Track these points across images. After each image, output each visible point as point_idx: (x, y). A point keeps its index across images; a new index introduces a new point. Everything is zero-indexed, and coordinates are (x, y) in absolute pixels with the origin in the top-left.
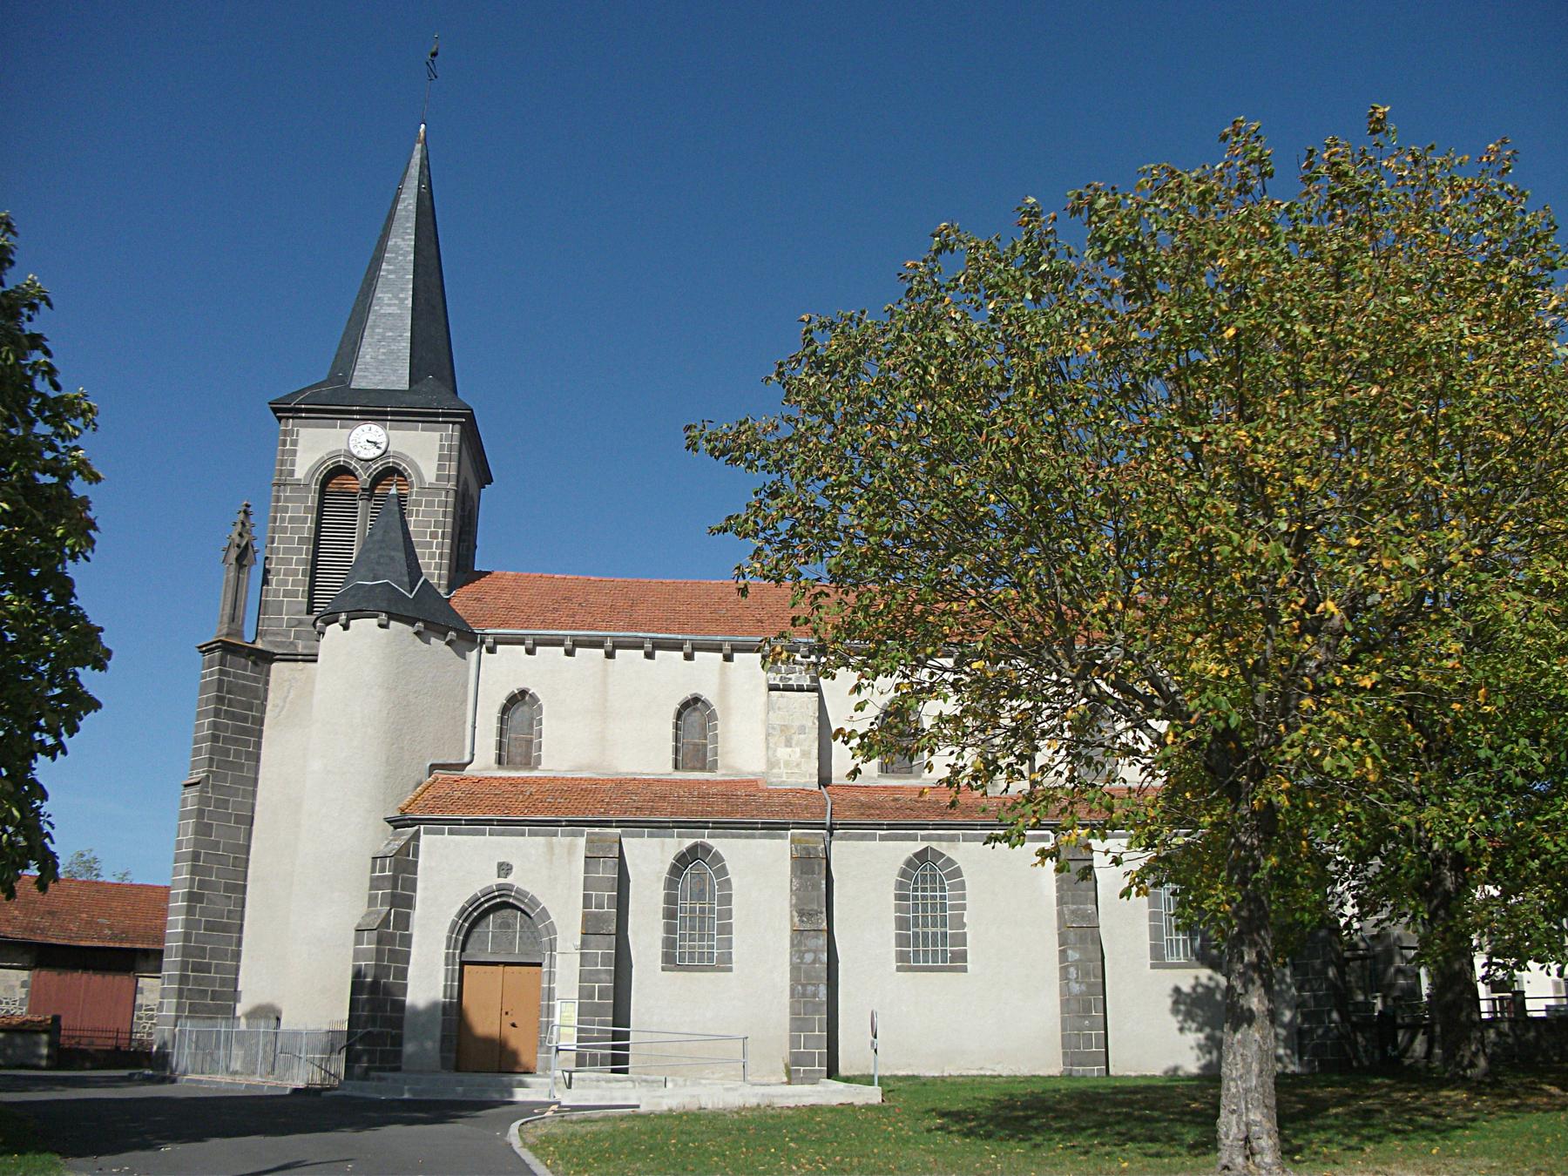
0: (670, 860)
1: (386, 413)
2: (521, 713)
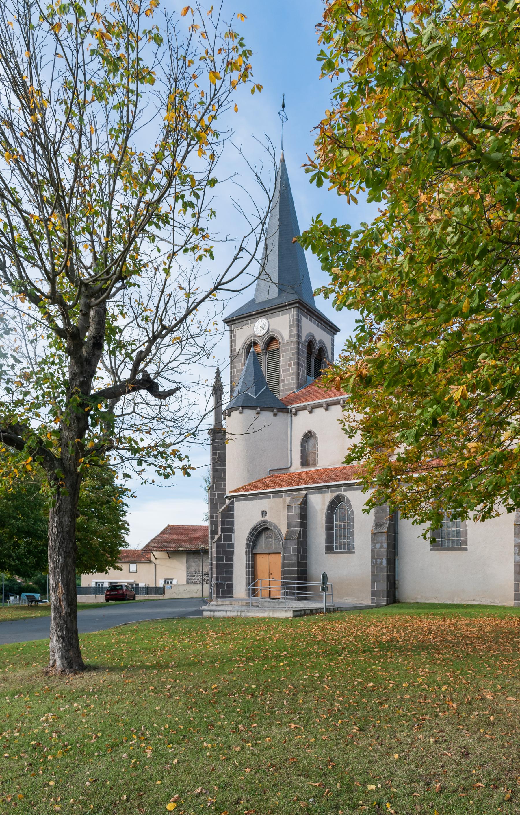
0: (327, 503)
1: (266, 311)
2: (311, 443)
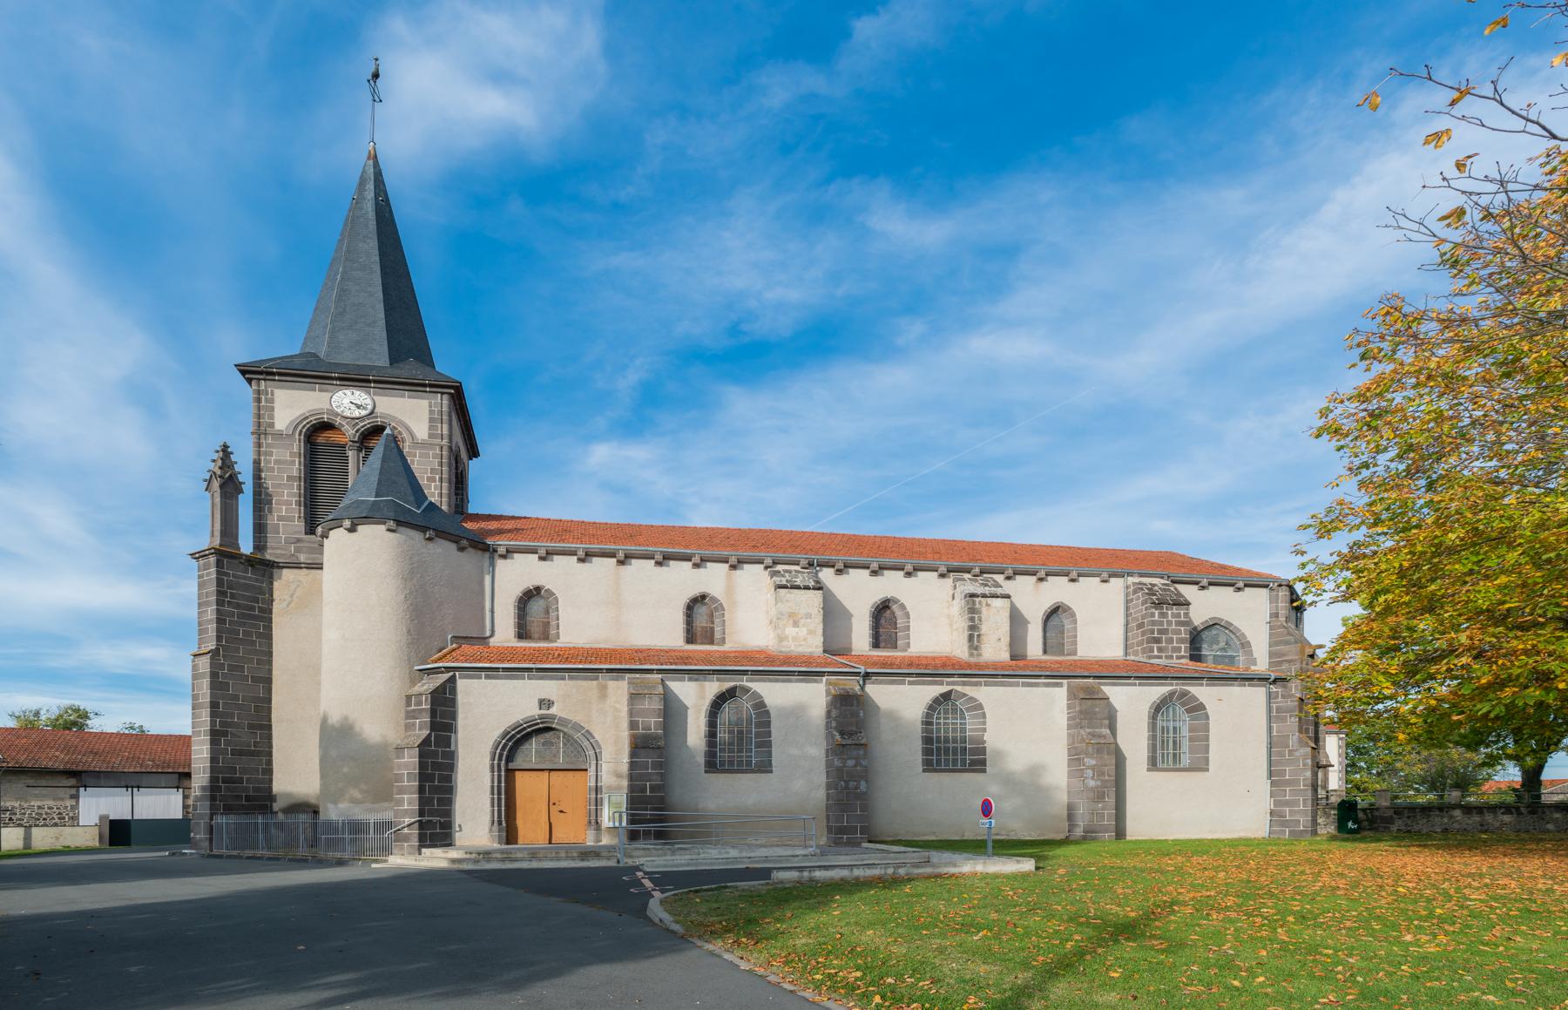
1: (369, 381)
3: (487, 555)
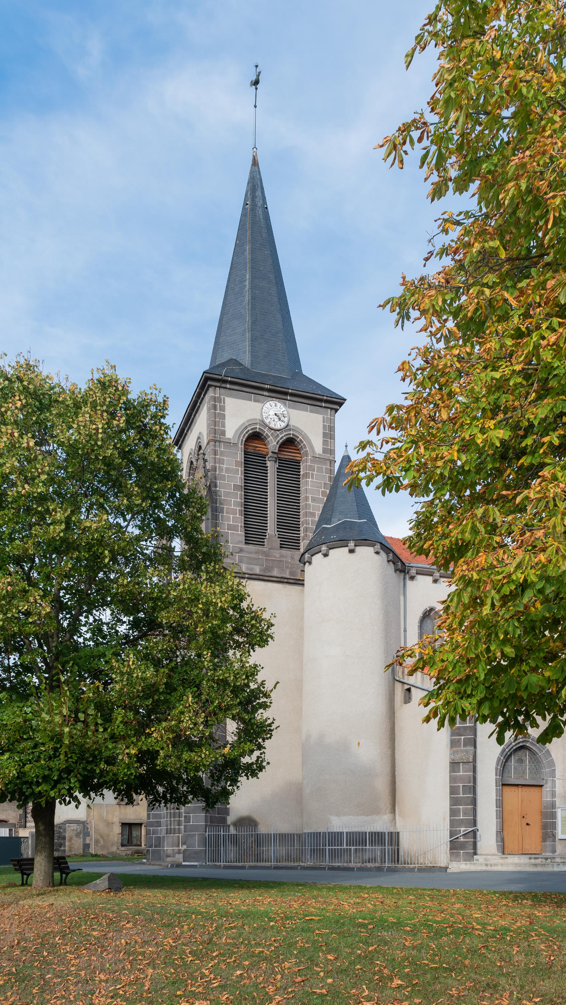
1: (286, 394)
3: (402, 574)
